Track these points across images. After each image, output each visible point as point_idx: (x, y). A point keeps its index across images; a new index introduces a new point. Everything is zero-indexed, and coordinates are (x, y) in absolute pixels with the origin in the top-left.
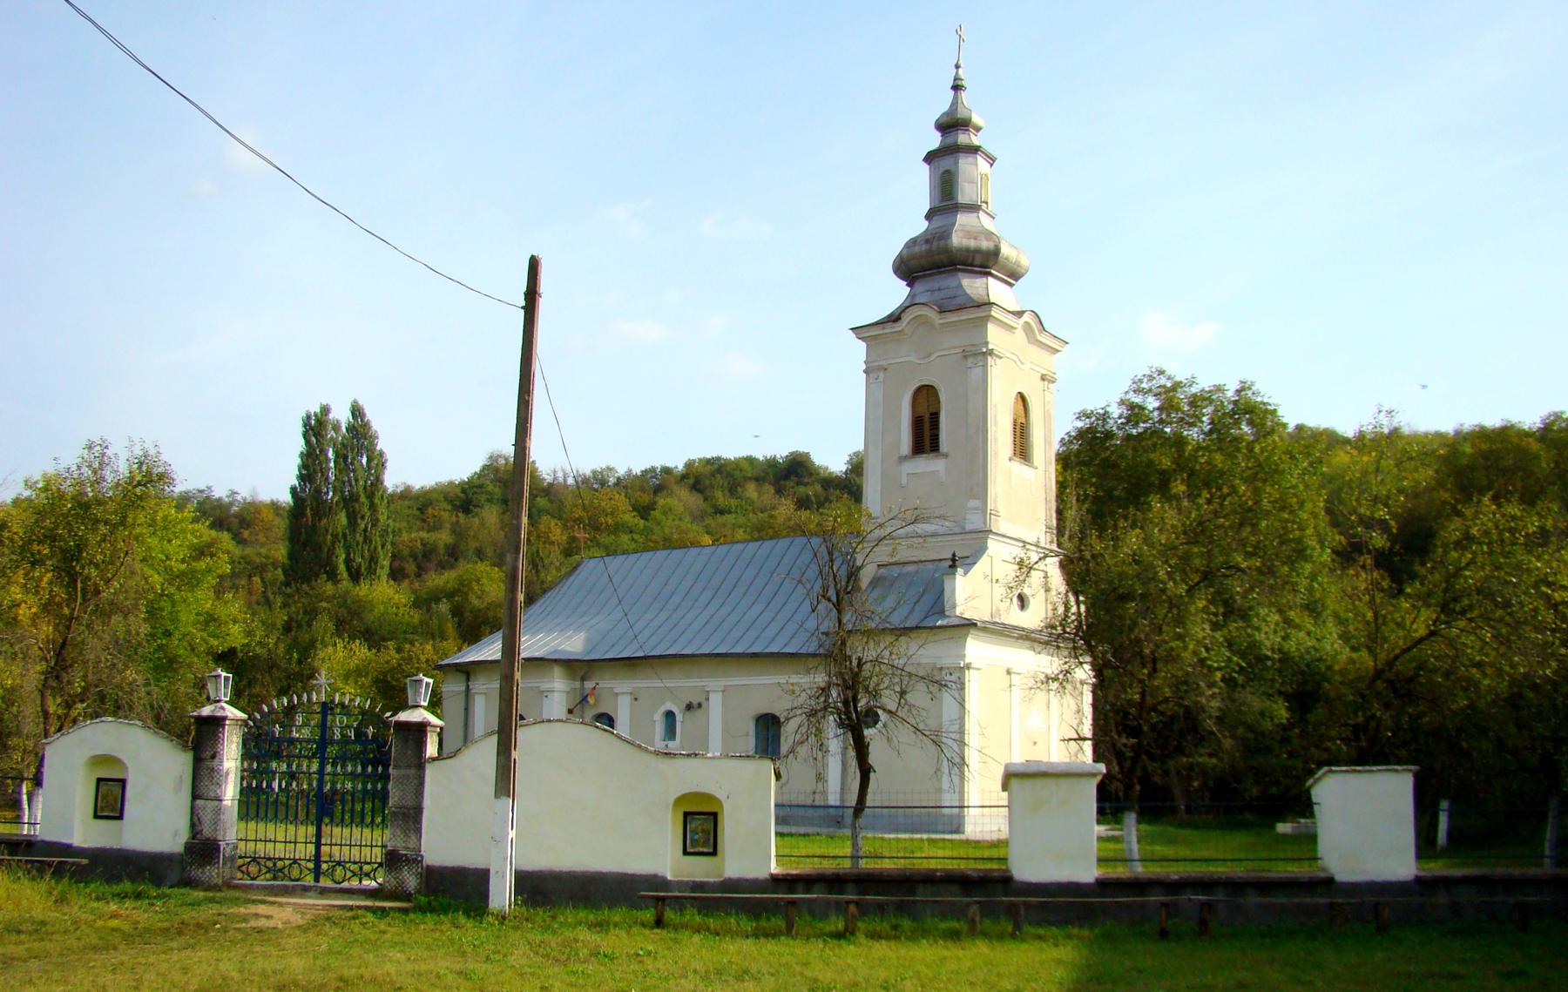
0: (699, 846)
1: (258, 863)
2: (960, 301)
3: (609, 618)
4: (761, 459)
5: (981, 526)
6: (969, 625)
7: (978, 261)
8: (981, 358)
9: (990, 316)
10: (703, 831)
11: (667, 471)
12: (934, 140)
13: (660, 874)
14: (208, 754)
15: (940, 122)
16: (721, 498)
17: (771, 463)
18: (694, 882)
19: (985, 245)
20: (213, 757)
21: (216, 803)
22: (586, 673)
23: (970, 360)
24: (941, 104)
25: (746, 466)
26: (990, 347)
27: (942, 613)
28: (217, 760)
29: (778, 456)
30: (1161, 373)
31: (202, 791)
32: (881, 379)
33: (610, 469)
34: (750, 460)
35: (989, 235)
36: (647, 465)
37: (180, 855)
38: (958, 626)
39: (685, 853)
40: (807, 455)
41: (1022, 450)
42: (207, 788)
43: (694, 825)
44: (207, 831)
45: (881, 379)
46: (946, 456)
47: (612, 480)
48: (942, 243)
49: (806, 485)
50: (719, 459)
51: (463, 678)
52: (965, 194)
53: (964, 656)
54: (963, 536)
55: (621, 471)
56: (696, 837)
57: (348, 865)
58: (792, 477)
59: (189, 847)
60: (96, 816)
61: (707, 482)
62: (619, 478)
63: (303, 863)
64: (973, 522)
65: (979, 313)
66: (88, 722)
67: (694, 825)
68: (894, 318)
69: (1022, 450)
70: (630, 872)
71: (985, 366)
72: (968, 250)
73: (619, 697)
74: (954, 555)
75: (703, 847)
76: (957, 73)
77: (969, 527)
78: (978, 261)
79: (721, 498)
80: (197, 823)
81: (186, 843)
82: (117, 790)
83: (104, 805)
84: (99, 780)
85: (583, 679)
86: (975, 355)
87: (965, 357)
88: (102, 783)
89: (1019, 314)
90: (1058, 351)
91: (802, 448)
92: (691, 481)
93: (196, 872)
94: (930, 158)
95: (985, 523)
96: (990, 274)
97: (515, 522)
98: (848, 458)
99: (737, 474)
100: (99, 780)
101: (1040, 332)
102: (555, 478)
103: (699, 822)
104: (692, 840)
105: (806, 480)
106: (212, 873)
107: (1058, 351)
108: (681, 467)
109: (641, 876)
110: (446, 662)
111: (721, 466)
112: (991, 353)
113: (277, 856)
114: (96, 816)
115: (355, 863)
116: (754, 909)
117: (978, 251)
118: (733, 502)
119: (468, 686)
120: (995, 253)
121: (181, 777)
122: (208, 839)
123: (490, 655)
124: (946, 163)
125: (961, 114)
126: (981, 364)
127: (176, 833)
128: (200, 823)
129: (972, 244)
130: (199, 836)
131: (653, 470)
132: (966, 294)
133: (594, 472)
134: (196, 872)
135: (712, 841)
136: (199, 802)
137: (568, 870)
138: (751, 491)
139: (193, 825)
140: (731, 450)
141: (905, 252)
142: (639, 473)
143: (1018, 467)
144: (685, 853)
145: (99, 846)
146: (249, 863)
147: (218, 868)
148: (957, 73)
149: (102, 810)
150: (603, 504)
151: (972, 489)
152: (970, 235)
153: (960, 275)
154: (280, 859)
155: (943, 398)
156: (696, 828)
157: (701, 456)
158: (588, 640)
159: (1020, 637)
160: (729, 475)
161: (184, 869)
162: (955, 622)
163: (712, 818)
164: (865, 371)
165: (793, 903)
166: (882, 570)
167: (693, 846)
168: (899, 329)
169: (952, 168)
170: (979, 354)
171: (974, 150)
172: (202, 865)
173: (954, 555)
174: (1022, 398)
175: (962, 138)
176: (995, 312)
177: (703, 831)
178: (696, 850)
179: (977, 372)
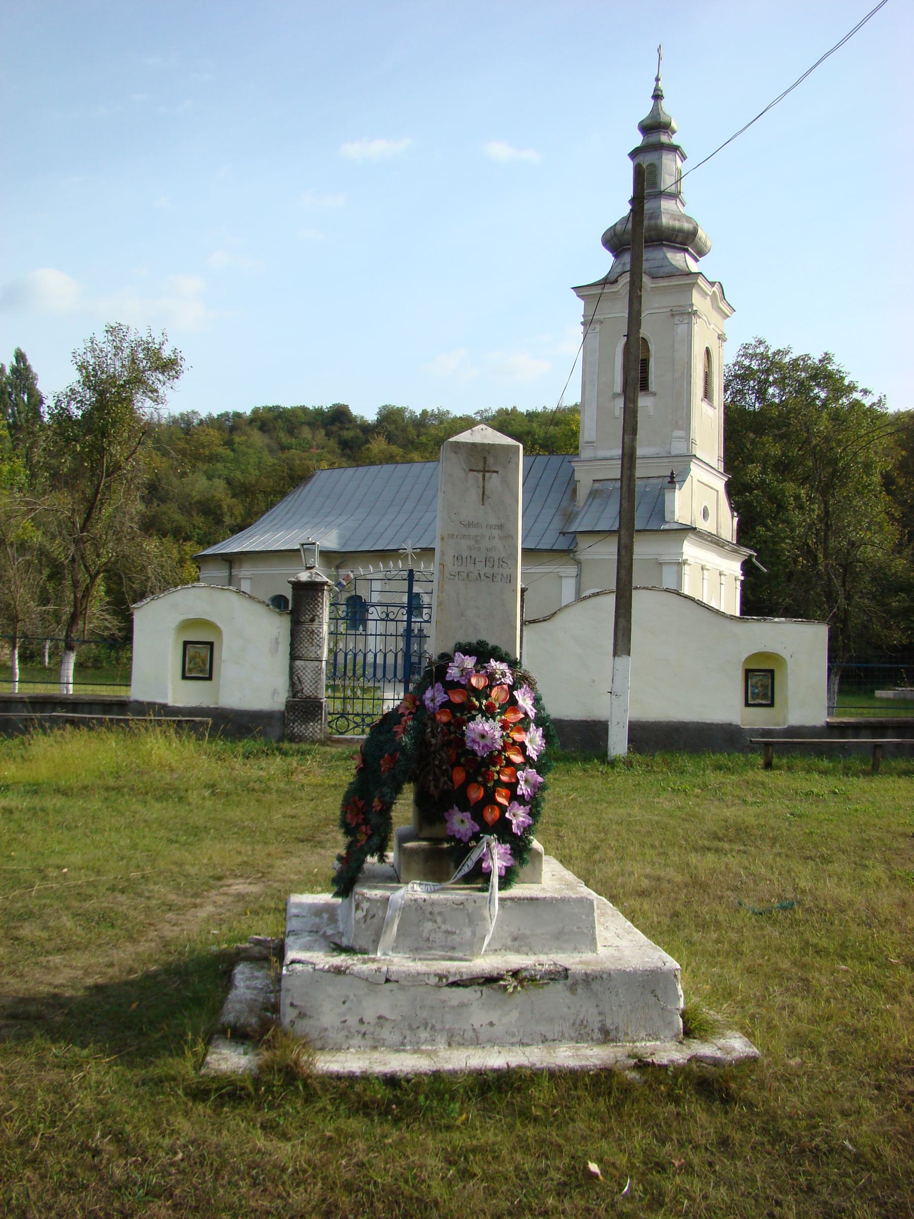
0: (757, 698)
1: (347, 719)
2: (666, 270)
3: (352, 518)
4: (311, 408)
5: (683, 451)
6: (689, 530)
7: (679, 239)
8: (686, 317)
9: (696, 283)
10: (762, 686)
11: (237, 415)
12: (638, 140)
13: (735, 723)
14: (308, 617)
15: (645, 123)
16: (285, 439)
17: (319, 412)
18: (763, 729)
19: (687, 226)
20: (312, 620)
21: (317, 663)
22: (342, 563)
23: (677, 318)
24: (644, 110)
25: (300, 413)
26: (695, 308)
27: (664, 521)
28: (316, 622)
29: (324, 407)
30: (761, 342)
31: (303, 652)
32: (597, 330)
33: (194, 413)
34: (304, 409)
35: (689, 219)
36: (222, 411)
37: (282, 713)
38: (676, 530)
39: (747, 704)
40: (385, 407)
41: (707, 395)
42: (306, 649)
43: (754, 680)
44: (308, 689)
45: (597, 330)
46: (655, 394)
47: (196, 422)
48: (653, 222)
49: (348, 429)
50: (278, 407)
51: (227, 565)
52: (667, 182)
53: (682, 553)
54: (671, 460)
55: (203, 415)
56: (756, 691)
57: (350, 717)
58: (337, 424)
59: (291, 706)
60: (184, 677)
61: (271, 425)
62: (201, 420)
63: (350, 717)
64: (678, 448)
65: (687, 281)
66: (179, 587)
67: (754, 680)
68: (606, 282)
69: (707, 395)
70: (708, 721)
71: (690, 324)
72: (673, 229)
73: (665, 568)
74: (672, 473)
75: (762, 699)
76: (657, 85)
77: (674, 452)
78: (679, 239)
79: (285, 439)
80: (297, 682)
81: (288, 702)
82: (205, 652)
83: (192, 666)
84: (186, 643)
85: (338, 567)
86: (682, 314)
87: (672, 315)
88: (189, 646)
89: (712, 284)
90: (728, 316)
91: (342, 401)
92: (259, 424)
93: (298, 729)
94: (633, 155)
95: (688, 450)
96: (687, 251)
97: (631, 406)
98: (378, 410)
99: (293, 419)
100: (186, 643)
101: (721, 300)
102: (152, 419)
103: (758, 678)
104: (753, 693)
105: (347, 426)
106: (315, 729)
107: (728, 316)
108: (248, 413)
109: (717, 725)
110: (209, 551)
111: (281, 413)
112: (695, 313)
113: (365, 712)
114: (184, 677)
115: (357, 715)
116: (820, 751)
117: (681, 231)
118: (293, 441)
119: (231, 573)
120: (694, 233)
121: (277, 639)
122: (309, 697)
123: (286, 543)
124: (647, 160)
125: (663, 119)
126: (686, 321)
127: (275, 692)
128: (300, 682)
129: (677, 224)
130: (299, 695)
131: (227, 414)
132: (671, 264)
133: (182, 415)
134: (298, 729)
135: (770, 694)
136: (298, 663)
137: (569, 719)
138: (306, 433)
139: (292, 685)
140: (288, 402)
141: (619, 228)
142: (216, 417)
143: (705, 406)
144: (747, 704)
145: (194, 705)
146: (338, 719)
147: (321, 724)
148: (657, 85)
149: (190, 670)
150: (202, 438)
151: (677, 422)
152: (674, 217)
153: (665, 249)
154: (368, 715)
155: (652, 348)
156: (757, 683)
157: (264, 405)
158: (341, 536)
159: (711, 542)
160: (287, 420)
161: (285, 726)
162: (675, 526)
163: (769, 674)
164: (583, 324)
165: (877, 746)
166: (597, 485)
167: (753, 699)
168: (615, 290)
169: (656, 162)
170: (688, 314)
171: (675, 149)
172: (306, 722)
173: (672, 473)
174: (707, 348)
175: (664, 139)
176: (700, 281)
177: (762, 686)
178: (756, 702)
179: (681, 329)
